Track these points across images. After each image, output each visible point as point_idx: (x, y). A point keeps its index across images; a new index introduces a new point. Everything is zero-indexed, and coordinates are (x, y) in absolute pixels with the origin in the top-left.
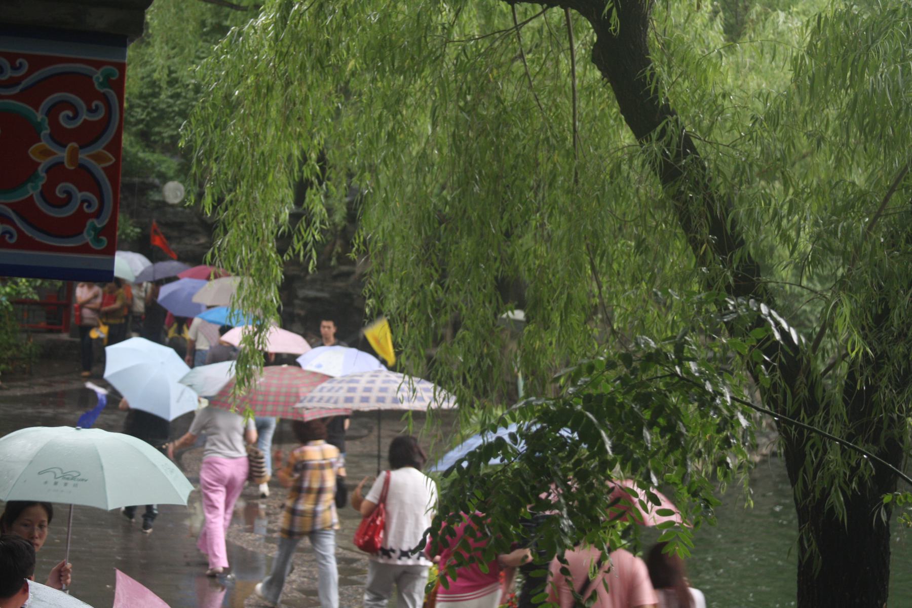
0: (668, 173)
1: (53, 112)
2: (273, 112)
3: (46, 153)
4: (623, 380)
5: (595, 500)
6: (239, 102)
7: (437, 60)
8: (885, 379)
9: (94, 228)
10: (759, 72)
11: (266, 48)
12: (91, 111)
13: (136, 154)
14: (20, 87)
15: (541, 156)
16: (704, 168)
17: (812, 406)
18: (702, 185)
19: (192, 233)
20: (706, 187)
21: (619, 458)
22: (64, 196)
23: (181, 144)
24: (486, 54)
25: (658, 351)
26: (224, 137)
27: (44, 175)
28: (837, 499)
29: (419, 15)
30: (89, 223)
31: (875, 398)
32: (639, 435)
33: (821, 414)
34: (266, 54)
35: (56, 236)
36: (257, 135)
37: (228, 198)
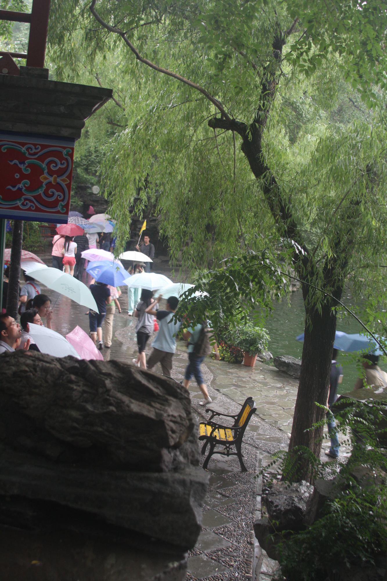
0: (266, 190)
1: (48, 164)
2: (130, 163)
3: (46, 178)
4: (244, 265)
5: (232, 307)
6: (118, 160)
7: (187, 147)
8: (338, 265)
9: (62, 205)
10: (301, 155)
11: (128, 141)
13: (83, 176)
14: (38, 155)
15: (223, 182)
16: (279, 189)
17: (312, 274)
18: (277, 195)
19: (102, 204)
20: (279, 196)
21: (241, 292)
22: (51, 194)
23: (97, 174)
24: (205, 146)
25: (256, 256)
26: (112, 172)
27: (45, 186)
28: (319, 306)
29: (181, 131)
30: (60, 203)
31: (334, 271)
32: (248, 285)
33: (315, 276)
34: (128, 143)
35: (49, 208)
36: (124, 171)
37: (113, 193)
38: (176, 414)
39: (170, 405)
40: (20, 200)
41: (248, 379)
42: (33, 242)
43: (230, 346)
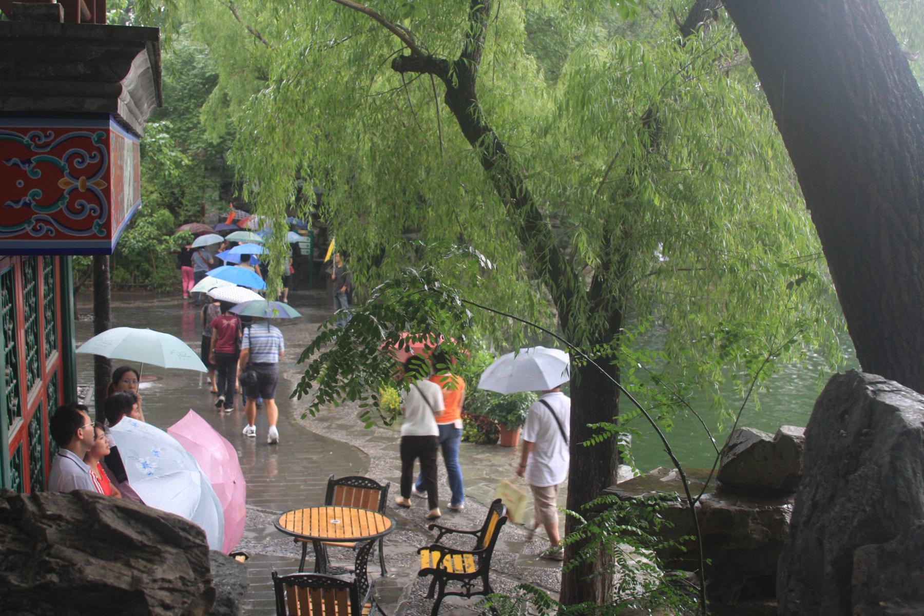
0: (487, 164)
9: (99, 225)
12: (91, 158)
38: (171, 576)
39: (162, 561)
40: (29, 222)
41: (507, 467)
42: (163, 278)
43: (476, 418)
